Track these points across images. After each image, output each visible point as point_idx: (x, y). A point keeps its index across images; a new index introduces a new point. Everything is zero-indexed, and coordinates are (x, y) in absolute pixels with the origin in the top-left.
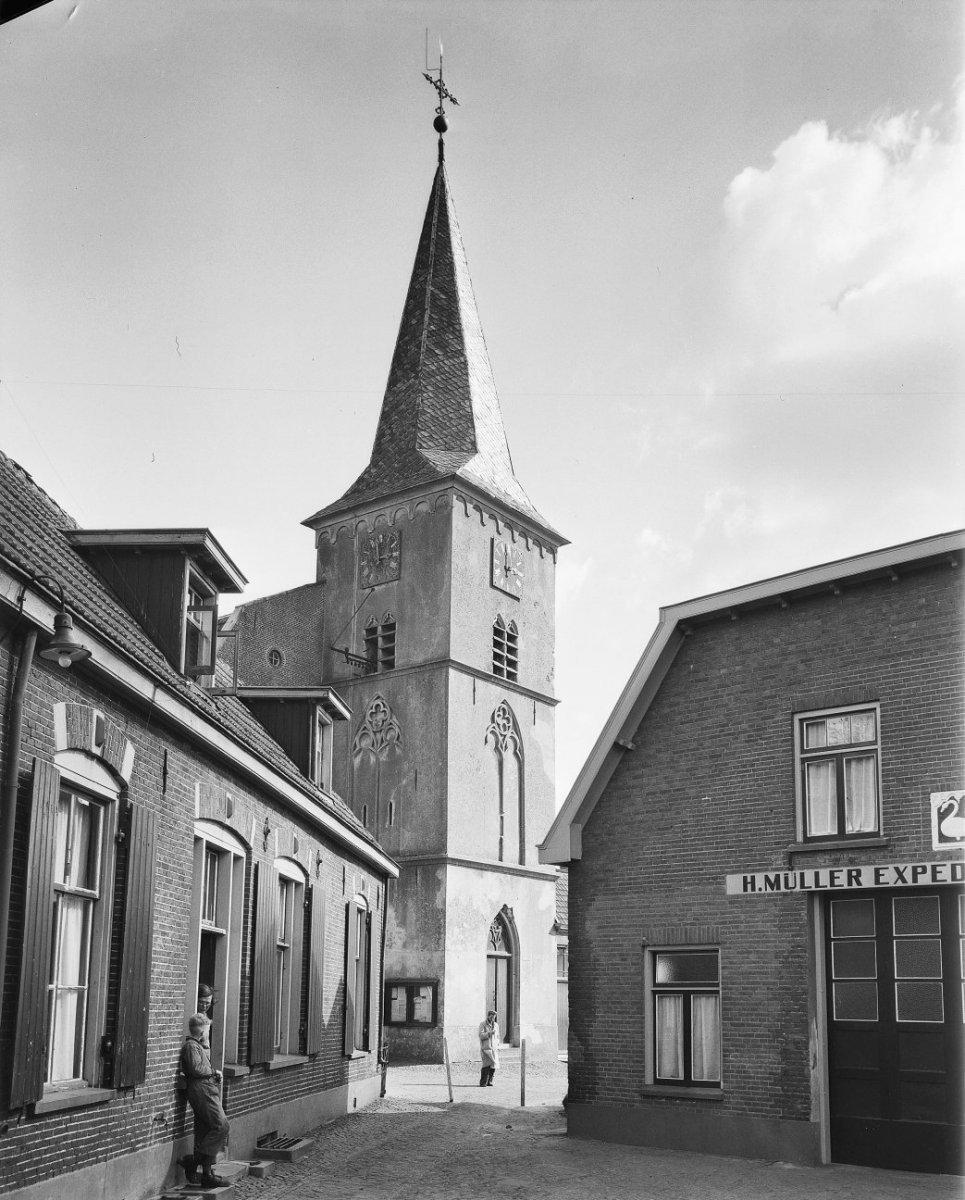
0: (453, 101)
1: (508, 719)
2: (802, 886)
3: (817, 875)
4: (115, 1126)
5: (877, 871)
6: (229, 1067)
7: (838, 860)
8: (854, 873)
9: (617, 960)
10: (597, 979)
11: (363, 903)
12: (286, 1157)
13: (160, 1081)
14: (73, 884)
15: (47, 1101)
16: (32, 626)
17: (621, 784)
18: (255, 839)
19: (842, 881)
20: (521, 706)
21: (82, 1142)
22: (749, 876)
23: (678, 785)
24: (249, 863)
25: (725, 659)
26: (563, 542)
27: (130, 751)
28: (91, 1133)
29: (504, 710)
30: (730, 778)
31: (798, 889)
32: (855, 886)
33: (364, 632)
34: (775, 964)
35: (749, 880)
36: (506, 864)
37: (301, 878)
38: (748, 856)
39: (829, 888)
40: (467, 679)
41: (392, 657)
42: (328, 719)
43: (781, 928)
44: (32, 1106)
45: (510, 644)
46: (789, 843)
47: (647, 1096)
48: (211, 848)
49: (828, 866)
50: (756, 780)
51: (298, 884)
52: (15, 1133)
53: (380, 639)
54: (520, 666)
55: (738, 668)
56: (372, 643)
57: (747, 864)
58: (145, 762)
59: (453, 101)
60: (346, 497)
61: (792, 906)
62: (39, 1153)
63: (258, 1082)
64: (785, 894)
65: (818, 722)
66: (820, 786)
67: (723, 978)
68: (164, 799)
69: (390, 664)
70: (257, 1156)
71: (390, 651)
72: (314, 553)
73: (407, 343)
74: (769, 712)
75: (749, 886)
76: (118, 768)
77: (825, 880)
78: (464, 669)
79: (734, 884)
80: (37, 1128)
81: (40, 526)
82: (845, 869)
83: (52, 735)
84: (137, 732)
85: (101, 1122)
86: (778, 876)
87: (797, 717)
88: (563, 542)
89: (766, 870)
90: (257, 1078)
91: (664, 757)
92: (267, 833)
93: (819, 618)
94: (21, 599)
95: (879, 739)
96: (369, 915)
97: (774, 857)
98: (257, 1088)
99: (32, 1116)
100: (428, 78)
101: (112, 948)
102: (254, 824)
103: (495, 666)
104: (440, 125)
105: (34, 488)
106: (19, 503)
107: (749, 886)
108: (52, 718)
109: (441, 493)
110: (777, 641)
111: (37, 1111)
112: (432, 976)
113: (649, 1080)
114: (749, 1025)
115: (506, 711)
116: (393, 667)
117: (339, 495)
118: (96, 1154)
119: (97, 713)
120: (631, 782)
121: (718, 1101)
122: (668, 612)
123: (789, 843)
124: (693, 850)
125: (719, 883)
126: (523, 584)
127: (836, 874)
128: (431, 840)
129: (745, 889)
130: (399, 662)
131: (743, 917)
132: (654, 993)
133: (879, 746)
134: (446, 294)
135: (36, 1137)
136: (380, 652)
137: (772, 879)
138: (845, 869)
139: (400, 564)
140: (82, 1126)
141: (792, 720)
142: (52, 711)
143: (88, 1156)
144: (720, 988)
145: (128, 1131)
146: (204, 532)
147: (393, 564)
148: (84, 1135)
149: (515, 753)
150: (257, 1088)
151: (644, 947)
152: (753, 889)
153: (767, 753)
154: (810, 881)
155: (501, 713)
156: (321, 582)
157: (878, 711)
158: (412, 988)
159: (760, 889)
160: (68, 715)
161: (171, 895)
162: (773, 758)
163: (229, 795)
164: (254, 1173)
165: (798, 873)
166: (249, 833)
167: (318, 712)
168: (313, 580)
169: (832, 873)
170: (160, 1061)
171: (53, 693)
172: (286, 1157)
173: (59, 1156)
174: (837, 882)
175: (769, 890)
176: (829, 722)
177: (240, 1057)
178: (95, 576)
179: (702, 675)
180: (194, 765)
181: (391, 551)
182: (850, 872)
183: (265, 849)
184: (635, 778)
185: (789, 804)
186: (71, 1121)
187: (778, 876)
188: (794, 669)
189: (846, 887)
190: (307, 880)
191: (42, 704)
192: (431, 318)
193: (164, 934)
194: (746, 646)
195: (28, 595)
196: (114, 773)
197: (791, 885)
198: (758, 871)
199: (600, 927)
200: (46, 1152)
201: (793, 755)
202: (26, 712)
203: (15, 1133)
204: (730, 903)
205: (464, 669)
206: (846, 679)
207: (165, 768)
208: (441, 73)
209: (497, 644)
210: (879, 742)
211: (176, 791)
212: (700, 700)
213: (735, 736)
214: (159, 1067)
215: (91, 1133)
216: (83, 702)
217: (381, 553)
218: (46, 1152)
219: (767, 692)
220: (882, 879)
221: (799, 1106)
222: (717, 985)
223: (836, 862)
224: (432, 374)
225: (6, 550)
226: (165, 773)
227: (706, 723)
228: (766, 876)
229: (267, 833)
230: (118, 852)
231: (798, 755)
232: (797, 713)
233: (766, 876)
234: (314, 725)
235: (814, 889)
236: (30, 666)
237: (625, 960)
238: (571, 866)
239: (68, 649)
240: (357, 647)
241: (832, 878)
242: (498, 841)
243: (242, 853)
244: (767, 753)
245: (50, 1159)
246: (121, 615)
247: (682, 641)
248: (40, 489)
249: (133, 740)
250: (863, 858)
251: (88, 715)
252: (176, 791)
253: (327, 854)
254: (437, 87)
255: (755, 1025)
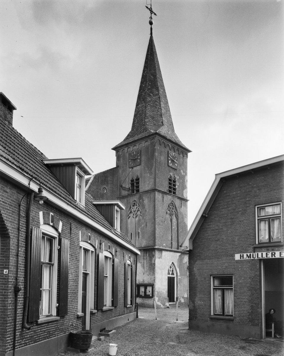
0: (155, 14)
1: (173, 206)
2: (258, 257)
3: (262, 254)
4: (60, 327)
5: (280, 253)
6: (92, 310)
7: (268, 249)
8: (273, 254)
9: (203, 279)
10: (197, 285)
11: (130, 262)
12: (108, 335)
13: (72, 315)
14: (47, 261)
15: (42, 319)
16: (32, 191)
17: (204, 227)
18: (97, 246)
19: (270, 256)
20: (177, 202)
21: (51, 331)
22: (242, 254)
23: (221, 227)
24: (96, 253)
25: (235, 191)
26: (190, 151)
27: (61, 223)
28: (53, 329)
29: (172, 203)
30: (236, 225)
31: (256, 258)
32: (273, 257)
33: (130, 181)
34: (250, 280)
35: (242, 256)
36: (173, 249)
37: (111, 256)
38: (241, 248)
39: (266, 258)
40: (161, 195)
41: (138, 189)
42: (119, 210)
43: (251, 270)
44: (37, 322)
45: (174, 183)
46: (254, 244)
47: (212, 319)
48: (85, 249)
49: (265, 251)
50: (244, 226)
51: (110, 258)
52: (33, 329)
53: (135, 183)
54: (177, 190)
55: (239, 192)
56: (132, 185)
57: (242, 251)
58: (65, 226)
59: (155, 14)
60: (124, 140)
61: (252, 262)
62: (40, 334)
63: (100, 315)
64: (252, 260)
65: (263, 208)
66: (264, 226)
67: (234, 284)
68: (71, 236)
69: (138, 191)
70: (100, 335)
71: (138, 187)
72: (115, 157)
73: (142, 92)
74: (248, 205)
75: (242, 257)
76: (57, 229)
77: (264, 255)
78: (159, 191)
79: (237, 257)
80: (39, 327)
81: (35, 160)
82: (271, 252)
83: (39, 221)
84: (62, 219)
85: (56, 326)
86: (250, 254)
87: (256, 207)
88: (190, 151)
89: (247, 253)
90: (100, 313)
91: (217, 219)
92: (100, 244)
93: (263, 176)
94: (29, 184)
95: (281, 213)
96: (132, 266)
97: (249, 249)
98: (99, 316)
99: (37, 324)
100: (147, 7)
101: (58, 264)
102: (97, 242)
103: (169, 190)
104: (151, 23)
105: (33, 147)
106: (29, 153)
107: (242, 257)
108: (39, 216)
109: (152, 138)
110: (250, 183)
111: (39, 323)
112: (152, 283)
113: (212, 314)
114: (242, 298)
115: (172, 204)
116: (139, 192)
117: (122, 140)
118: (55, 334)
119: (51, 213)
120: (207, 227)
121: (232, 320)
122: (218, 176)
123: (254, 244)
124: (225, 247)
125: (233, 257)
126: (178, 165)
127: (268, 254)
128: (151, 243)
129: (241, 258)
130: (141, 190)
131: (240, 266)
132: (214, 289)
133: (281, 215)
134: (153, 76)
135: (39, 330)
136: (135, 187)
137: (249, 255)
138: (271, 252)
139: (140, 160)
140: (51, 327)
141: (255, 207)
142: (39, 214)
143: (53, 335)
144: (233, 287)
145: (63, 328)
146: (81, 158)
147: (139, 160)
148: (52, 329)
149: (176, 216)
150: (99, 316)
151: (211, 275)
152: (243, 258)
153: (247, 218)
154: (260, 256)
155: (171, 204)
156: (118, 166)
157: (281, 204)
158: (146, 286)
159: (245, 258)
160: (43, 214)
161: (74, 263)
162: (249, 219)
163: (89, 234)
164: (100, 340)
165: (256, 253)
166: (95, 244)
167: (115, 208)
168: (115, 166)
169: (267, 253)
170: (72, 309)
171: (39, 209)
172: (108, 335)
173: (45, 335)
174: (268, 256)
175: (248, 259)
176: (266, 208)
177: (94, 308)
178: (50, 172)
179: (228, 194)
180: (79, 226)
181: (138, 156)
182: (272, 253)
183: (100, 249)
184: (208, 225)
185: (252, 233)
186: (48, 325)
187: (250, 254)
188: (255, 192)
189: (271, 257)
190: (113, 257)
191: (36, 212)
192: (149, 84)
193: (72, 274)
194: (241, 185)
195: (31, 183)
196: (57, 230)
197: (254, 257)
198: (244, 253)
199: (198, 270)
200: (41, 334)
201: (255, 218)
202: (32, 214)
203: (33, 329)
204: (237, 262)
205: (159, 191)
206: (271, 195)
207: (71, 228)
208: (151, 6)
209: (170, 184)
210: (281, 214)
211: (74, 234)
212: (227, 202)
213: (238, 212)
214: (72, 311)
215: (53, 329)
216: (47, 211)
217: (135, 160)
218: (41, 334)
219: (248, 199)
220: (282, 255)
221: (256, 322)
222: (232, 286)
223: (268, 250)
224: (150, 101)
225: (25, 170)
226: (71, 229)
227: (229, 209)
228: (247, 255)
229: (100, 244)
230: (58, 252)
231: (257, 218)
232: (256, 205)
233: (247, 255)
234: (114, 212)
235: (261, 258)
236: (32, 202)
237: (205, 279)
238: (191, 253)
239: (42, 198)
240: (128, 185)
241: (267, 255)
242: (171, 243)
243: (93, 250)
244: (247, 218)
245: (43, 336)
246: (58, 184)
247: (222, 184)
248: (35, 147)
249: (62, 220)
250: (276, 249)
251: (49, 214)
252: (74, 234)
253: (118, 249)
254: (150, 10)
255: (243, 298)
